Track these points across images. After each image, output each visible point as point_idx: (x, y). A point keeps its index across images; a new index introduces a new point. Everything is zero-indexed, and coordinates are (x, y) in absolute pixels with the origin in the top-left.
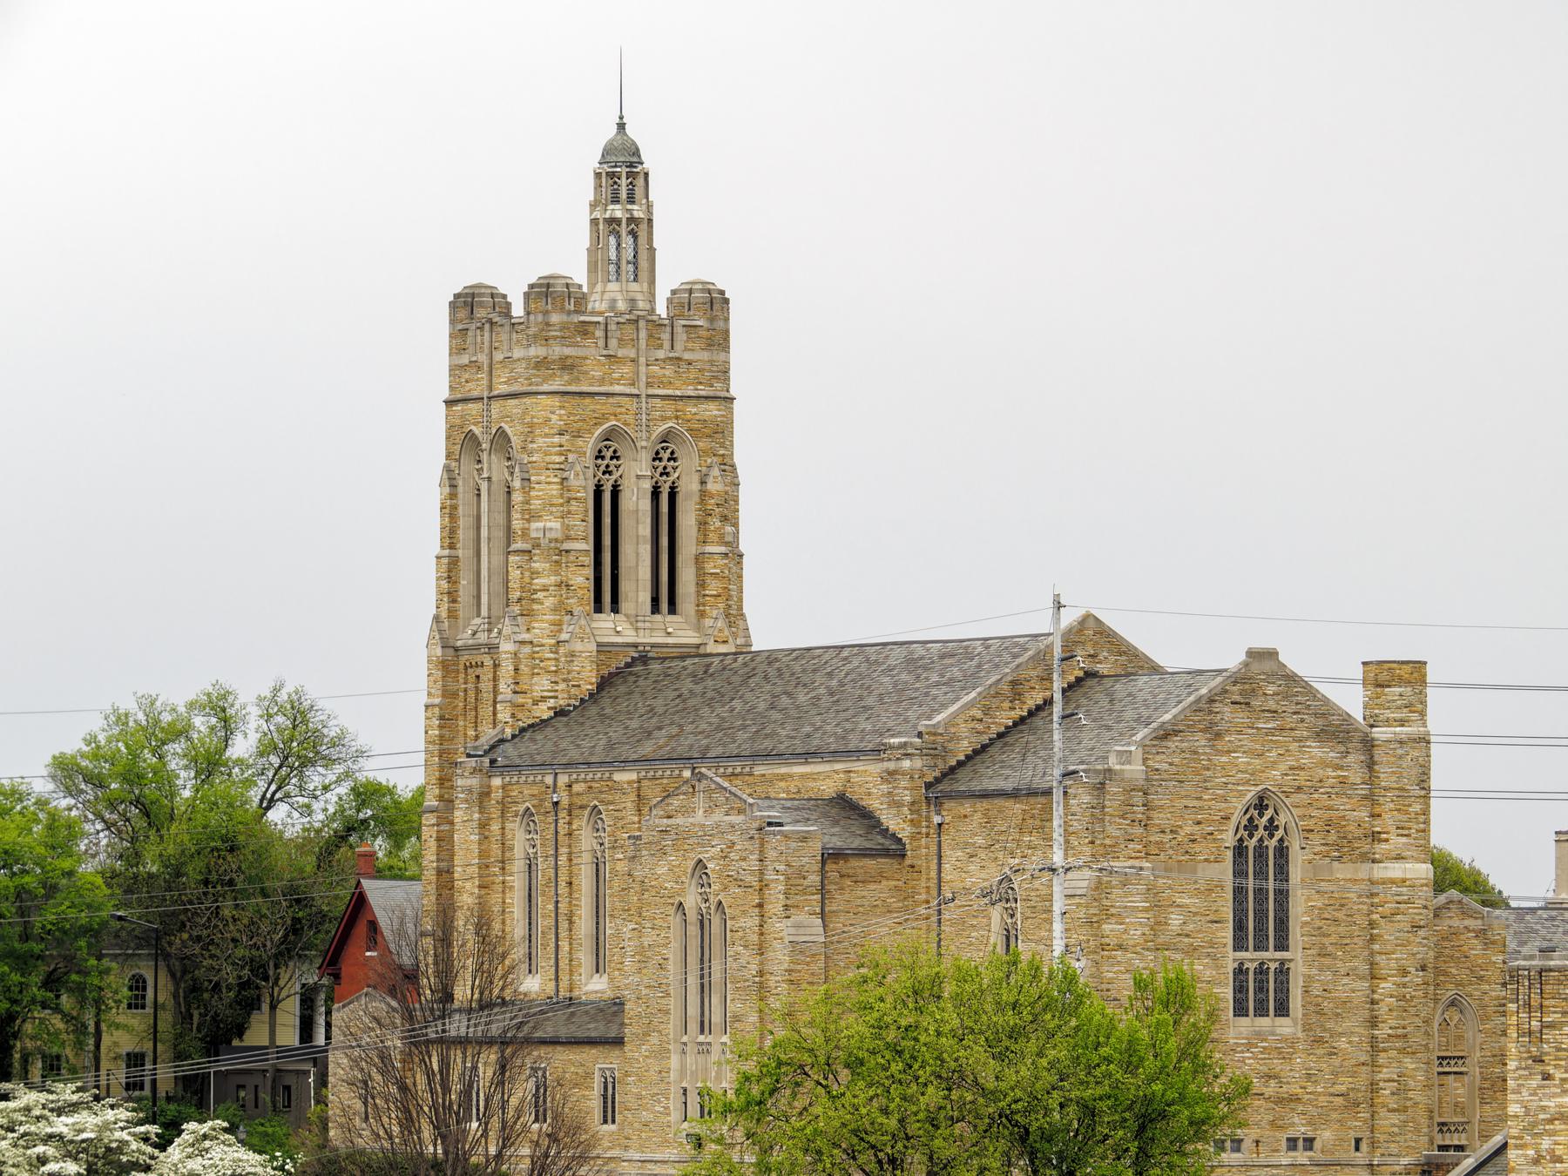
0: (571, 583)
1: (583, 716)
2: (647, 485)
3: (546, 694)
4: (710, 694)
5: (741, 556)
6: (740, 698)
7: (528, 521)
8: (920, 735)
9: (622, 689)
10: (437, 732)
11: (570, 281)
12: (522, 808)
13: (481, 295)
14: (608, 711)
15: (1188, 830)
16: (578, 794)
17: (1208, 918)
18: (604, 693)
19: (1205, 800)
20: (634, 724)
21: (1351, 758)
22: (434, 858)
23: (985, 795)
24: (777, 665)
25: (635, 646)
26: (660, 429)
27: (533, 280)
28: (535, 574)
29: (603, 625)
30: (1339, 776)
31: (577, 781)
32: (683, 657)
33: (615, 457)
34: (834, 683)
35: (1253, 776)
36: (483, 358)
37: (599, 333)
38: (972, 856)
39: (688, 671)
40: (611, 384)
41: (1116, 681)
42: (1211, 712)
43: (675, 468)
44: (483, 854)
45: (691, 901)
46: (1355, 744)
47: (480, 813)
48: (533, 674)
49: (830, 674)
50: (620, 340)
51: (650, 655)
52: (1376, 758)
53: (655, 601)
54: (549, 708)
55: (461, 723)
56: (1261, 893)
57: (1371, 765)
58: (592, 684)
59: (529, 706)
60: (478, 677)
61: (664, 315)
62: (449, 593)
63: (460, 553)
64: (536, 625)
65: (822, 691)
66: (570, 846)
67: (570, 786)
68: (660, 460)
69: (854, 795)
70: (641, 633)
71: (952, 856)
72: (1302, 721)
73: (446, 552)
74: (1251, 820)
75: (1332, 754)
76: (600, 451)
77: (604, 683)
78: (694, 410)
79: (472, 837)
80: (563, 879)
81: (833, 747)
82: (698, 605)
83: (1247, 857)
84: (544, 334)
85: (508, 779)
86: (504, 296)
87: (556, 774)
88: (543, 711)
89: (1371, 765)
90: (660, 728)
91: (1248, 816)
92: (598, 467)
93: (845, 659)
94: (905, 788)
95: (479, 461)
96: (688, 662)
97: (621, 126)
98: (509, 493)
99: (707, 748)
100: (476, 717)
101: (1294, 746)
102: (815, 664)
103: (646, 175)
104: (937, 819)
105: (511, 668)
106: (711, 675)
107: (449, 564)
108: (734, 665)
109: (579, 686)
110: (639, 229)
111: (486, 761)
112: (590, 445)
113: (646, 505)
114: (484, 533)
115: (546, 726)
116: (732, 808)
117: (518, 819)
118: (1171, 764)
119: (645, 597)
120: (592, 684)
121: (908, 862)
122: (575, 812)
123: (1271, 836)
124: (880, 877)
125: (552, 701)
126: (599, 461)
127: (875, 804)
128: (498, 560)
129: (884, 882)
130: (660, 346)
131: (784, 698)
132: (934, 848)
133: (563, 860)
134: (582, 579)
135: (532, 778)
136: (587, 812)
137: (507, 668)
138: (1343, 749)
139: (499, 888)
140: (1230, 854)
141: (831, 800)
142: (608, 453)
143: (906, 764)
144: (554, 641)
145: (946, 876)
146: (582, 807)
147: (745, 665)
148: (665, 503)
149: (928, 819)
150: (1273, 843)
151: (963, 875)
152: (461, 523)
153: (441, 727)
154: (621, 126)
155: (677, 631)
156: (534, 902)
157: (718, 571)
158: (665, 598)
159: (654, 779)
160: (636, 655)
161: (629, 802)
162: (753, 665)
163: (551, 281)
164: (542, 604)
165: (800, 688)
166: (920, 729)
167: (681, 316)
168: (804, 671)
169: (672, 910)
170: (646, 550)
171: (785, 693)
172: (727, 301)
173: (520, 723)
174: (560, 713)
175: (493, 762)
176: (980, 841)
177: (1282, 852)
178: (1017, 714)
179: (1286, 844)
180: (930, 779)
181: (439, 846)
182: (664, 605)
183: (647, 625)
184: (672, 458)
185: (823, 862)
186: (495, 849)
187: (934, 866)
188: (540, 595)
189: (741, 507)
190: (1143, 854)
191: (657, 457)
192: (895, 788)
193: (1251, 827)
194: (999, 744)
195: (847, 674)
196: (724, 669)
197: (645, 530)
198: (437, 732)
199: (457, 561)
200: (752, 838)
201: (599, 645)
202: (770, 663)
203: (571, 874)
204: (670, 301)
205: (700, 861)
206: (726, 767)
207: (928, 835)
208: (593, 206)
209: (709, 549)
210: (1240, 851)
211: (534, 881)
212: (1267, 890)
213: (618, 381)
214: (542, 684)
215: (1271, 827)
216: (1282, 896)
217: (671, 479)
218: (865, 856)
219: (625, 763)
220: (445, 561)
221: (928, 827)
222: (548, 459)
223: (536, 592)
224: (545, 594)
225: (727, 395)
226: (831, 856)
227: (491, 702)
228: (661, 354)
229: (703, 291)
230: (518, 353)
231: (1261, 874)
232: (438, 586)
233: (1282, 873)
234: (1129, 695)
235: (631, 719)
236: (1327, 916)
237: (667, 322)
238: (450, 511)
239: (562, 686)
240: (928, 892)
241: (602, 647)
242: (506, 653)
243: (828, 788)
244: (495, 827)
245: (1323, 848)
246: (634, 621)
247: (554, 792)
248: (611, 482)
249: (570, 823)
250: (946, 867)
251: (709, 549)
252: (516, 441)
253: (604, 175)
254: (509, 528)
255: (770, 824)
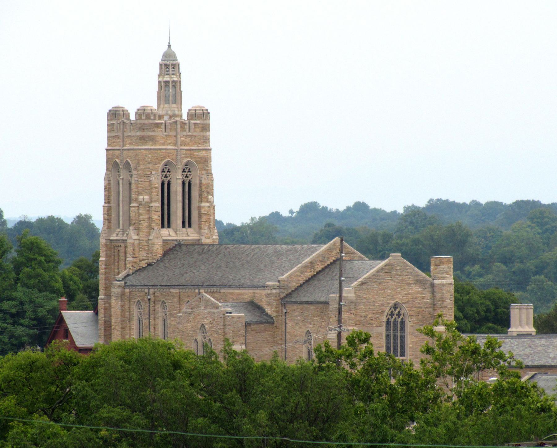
0: (153, 218)
1: (158, 266)
2: (180, 182)
3: (144, 258)
4: (205, 260)
5: (214, 206)
6: (215, 262)
7: (138, 195)
8: (279, 281)
9: (172, 256)
10: (104, 270)
11: (152, 108)
12: (137, 300)
13: (118, 111)
14: (167, 265)
15: (370, 316)
16: (157, 296)
17: (377, 346)
18: (165, 258)
19: (376, 306)
20: (177, 271)
21: (426, 291)
22: (103, 316)
23: (301, 303)
24: (228, 250)
25: (176, 240)
26: (185, 161)
27: (138, 107)
28: (140, 214)
29: (164, 232)
30: (422, 297)
31: (157, 292)
32: (193, 245)
33: (169, 171)
34: (249, 259)
35: (393, 298)
36: (120, 134)
37: (163, 127)
38: (297, 324)
39: (196, 251)
40: (167, 145)
41: (347, 262)
42: (378, 276)
43: (190, 175)
44: (123, 317)
45: (199, 338)
46: (428, 285)
47: (121, 301)
48: (140, 251)
49: (247, 255)
50: (170, 129)
51: (182, 243)
52: (435, 290)
53: (183, 223)
54: (146, 263)
55: (113, 267)
56: (395, 336)
57: (433, 292)
58: (161, 254)
59: (138, 262)
60: (119, 250)
61: (186, 119)
62: (108, 220)
63: (112, 205)
64: (141, 233)
65: (245, 261)
66: (154, 314)
67: (154, 293)
68: (185, 172)
69: (256, 301)
70: (179, 235)
71: (290, 324)
72: (410, 278)
73: (107, 205)
74: (392, 312)
75: (420, 289)
76: (163, 169)
77: (165, 254)
78: (197, 154)
79: (118, 310)
80: (152, 327)
81: (249, 284)
82: (199, 225)
83: (390, 324)
84: (143, 127)
85: (131, 290)
86: (127, 111)
87: (149, 289)
88: (143, 264)
89: (433, 292)
90: (186, 273)
91: (391, 311)
92: (162, 175)
93: (252, 249)
94: (274, 300)
95: (119, 172)
96: (196, 247)
97: (169, 46)
98: (130, 184)
99: (204, 282)
100: (118, 265)
101: (406, 287)
102: (242, 251)
103: (179, 64)
104: (284, 311)
105: (132, 249)
106: (205, 253)
107: (108, 209)
108: (212, 249)
109: (156, 255)
110: (176, 85)
111: (123, 282)
112: (160, 168)
113: (180, 189)
114: (121, 198)
115: (144, 270)
116: (214, 307)
117: (135, 304)
118: (364, 294)
119: (180, 222)
120: (161, 254)
121: (275, 325)
122: (156, 302)
123: (399, 317)
124: (266, 330)
125: (147, 260)
126: (163, 173)
127: (263, 304)
128: (126, 208)
129: (267, 332)
130: (185, 131)
131: (231, 263)
132: (284, 320)
133: (152, 320)
134: (157, 216)
135: (140, 290)
136: (160, 303)
137: (130, 249)
138: (424, 287)
139: (128, 328)
140: (384, 324)
141: (248, 302)
142: (167, 170)
143: (274, 291)
144: (147, 239)
145: (288, 330)
146: (160, 301)
147: (217, 249)
148: (187, 188)
149: (282, 311)
150: (399, 320)
151: (294, 330)
152: (112, 193)
153: (105, 268)
154: (169, 46)
155: (190, 235)
156: (141, 334)
157: (206, 212)
158: (187, 222)
159: (185, 292)
160: (177, 243)
161: (176, 300)
162: (219, 250)
163: (145, 108)
164: (143, 225)
165: (236, 260)
166: (279, 279)
167: (192, 119)
168: (238, 253)
169: (193, 341)
170: (180, 205)
171: (231, 262)
172: (209, 113)
173: (135, 269)
174: (149, 265)
175: (125, 283)
176: (299, 318)
177: (403, 323)
178: (312, 273)
179: (404, 320)
180: (282, 296)
181: (105, 312)
182: (187, 224)
183: (181, 232)
184: (189, 171)
185: (246, 326)
186: (127, 315)
187: (284, 327)
188: (142, 222)
189: (214, 188)
190: (354, 325)
191: (184, 171)
192: (270, 299)
193: (392, 314)
194: (306, 284)
195: (253, 256)
196: (209, 251)
197: (180, 198)
198: (104, 270)
199: (111, 208)
200: (221, 317)
201: (164, 240)
202: (226, 249)
203: (155, 324)
204: (188, 114)
205: (203, 324)
206: (211, 289)
207: (281, 316)
208: (159, 76)
209: (203, 204)
210: (388, 322)
211: (141, 327)
212: (397, 336)
213: (169, 144)
214: (143, 254)
215: (399, 314)
216: (403, 338)
217: (189, 179)
218: (260, 323)
219: (174, 286)
220: (106, 208)
221: (282, 313)
222: (145, 173)
223: (140, 221)
224: (144, 222)
225: (209, 148)
226: (247, 324)
227: (124, 260)
228: (185, 134)
229: (200, 110)
230: (133, 134)
231: (395, 330)
232: (104, 217)
233: (403, 328)
234: (351, 268)
235: (176, 269)
236: (418, 344)
237: (187, 122)
238: (108, 189)
239: (150, 255)
240: (282, 336)
241: (165, 241)
242: (130, 243)
243: (247, 298)
244: (127, 307)
245: (416, 321)
246: (176, 232)
247: (149, 295)
248: (167, 181)
249: (154, 306)
250: (288, 327)
251: (203, 204)
252: (132, 166)
253: (163, 65)
254: (130, 197)
255: (227, 313)
